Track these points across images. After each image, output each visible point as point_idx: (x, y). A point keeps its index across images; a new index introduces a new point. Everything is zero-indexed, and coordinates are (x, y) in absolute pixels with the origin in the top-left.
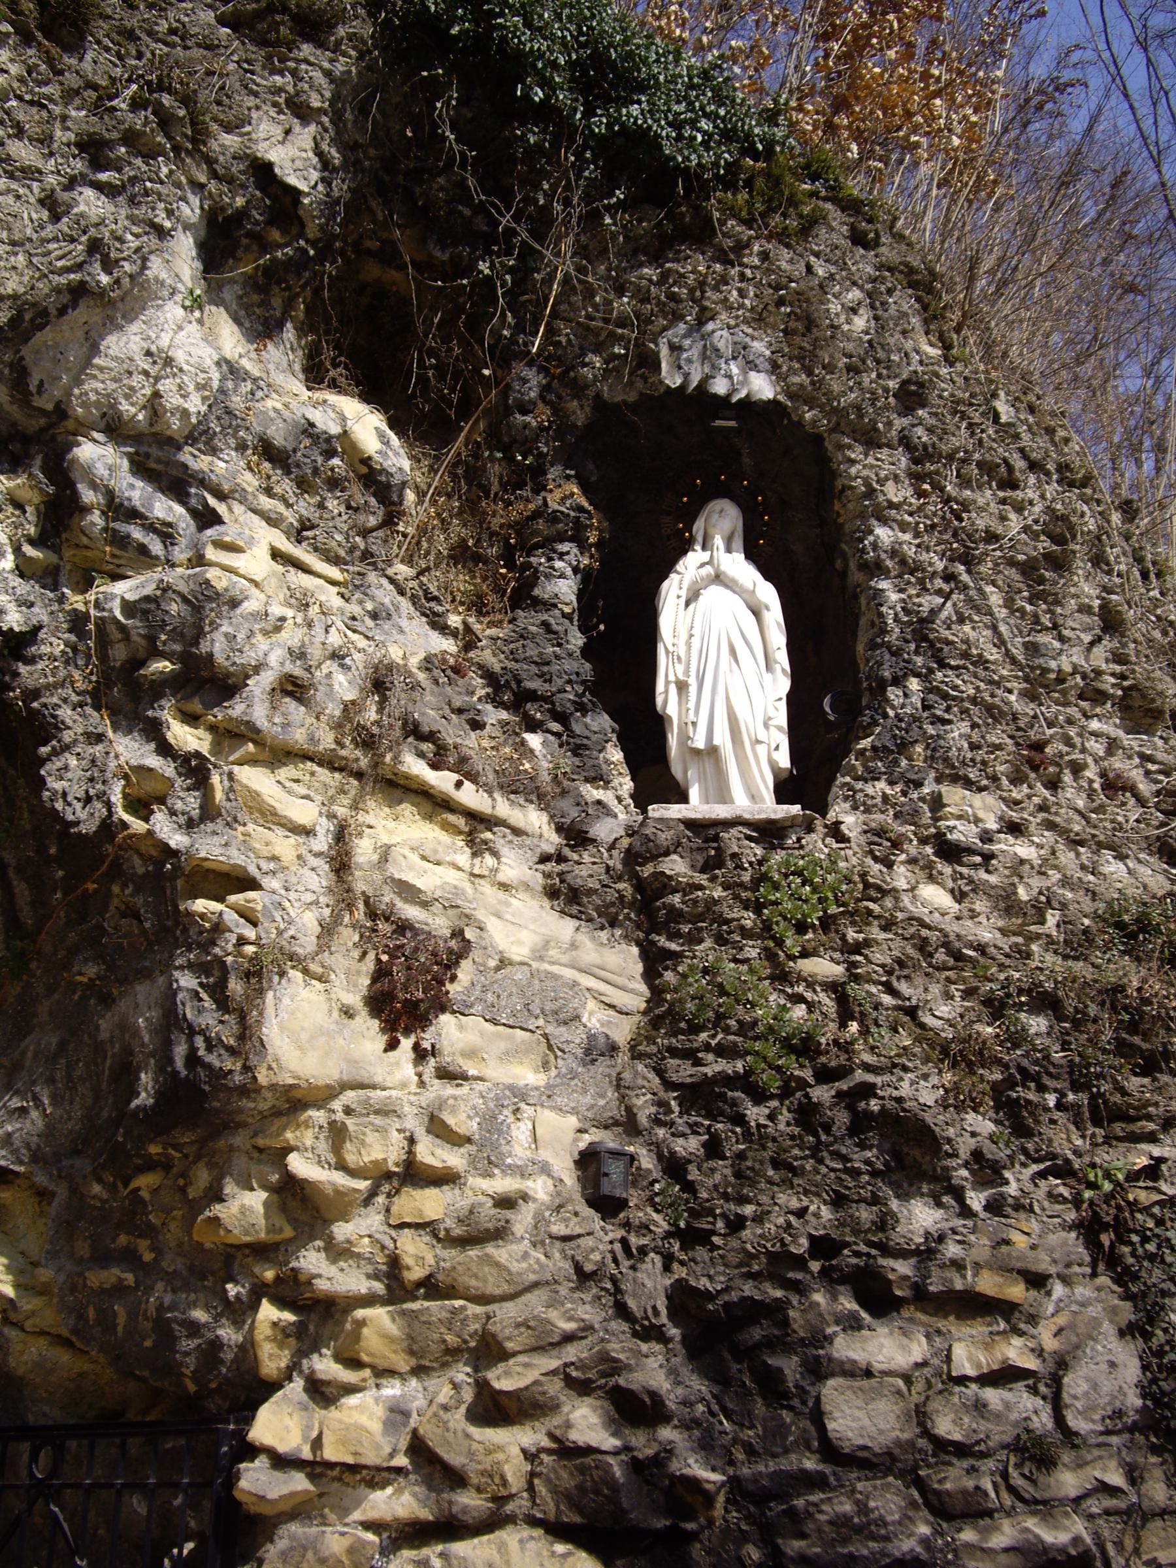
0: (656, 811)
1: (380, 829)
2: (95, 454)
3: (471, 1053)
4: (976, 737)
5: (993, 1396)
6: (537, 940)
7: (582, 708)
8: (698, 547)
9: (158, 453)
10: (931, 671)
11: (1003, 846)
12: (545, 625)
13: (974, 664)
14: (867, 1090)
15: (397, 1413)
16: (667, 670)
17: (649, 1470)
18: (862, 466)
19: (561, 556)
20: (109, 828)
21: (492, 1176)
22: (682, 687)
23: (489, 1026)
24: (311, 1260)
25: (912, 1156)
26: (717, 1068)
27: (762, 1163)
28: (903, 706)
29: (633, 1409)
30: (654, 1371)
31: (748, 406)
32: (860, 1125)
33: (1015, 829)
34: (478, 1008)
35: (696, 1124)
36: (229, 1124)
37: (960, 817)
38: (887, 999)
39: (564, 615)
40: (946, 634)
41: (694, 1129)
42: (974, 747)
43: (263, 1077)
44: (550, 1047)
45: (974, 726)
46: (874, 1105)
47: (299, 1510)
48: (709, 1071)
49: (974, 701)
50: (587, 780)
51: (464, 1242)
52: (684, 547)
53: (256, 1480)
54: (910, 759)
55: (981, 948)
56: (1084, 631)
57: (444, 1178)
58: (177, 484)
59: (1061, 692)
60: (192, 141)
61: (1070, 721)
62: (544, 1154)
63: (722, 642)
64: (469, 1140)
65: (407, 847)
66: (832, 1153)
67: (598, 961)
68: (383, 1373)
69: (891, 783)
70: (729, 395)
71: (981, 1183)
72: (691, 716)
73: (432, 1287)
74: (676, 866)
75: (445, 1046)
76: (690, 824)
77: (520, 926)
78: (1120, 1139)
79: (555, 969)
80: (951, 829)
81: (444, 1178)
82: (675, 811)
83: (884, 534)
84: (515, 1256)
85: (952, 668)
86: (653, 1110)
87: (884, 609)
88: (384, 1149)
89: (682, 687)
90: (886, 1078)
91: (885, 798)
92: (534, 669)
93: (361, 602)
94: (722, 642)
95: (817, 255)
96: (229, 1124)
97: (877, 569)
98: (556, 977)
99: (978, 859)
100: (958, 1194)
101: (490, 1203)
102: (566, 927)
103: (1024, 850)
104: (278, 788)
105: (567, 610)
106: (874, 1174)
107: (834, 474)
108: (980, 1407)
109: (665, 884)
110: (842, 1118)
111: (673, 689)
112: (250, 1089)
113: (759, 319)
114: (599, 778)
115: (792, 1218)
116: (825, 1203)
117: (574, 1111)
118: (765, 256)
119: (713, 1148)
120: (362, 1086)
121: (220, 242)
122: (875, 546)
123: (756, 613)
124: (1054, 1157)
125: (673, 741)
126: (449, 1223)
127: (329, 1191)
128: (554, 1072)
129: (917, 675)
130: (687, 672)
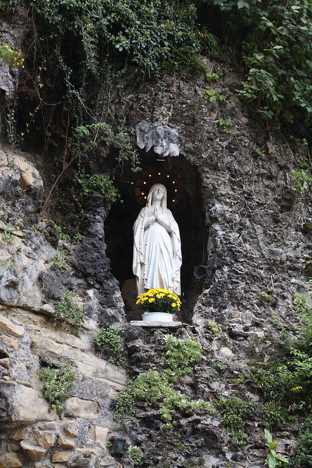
0: (134, 323)
1: (42, 332)
3: (76, 410)
4: (247, 289)
6: (94, 369)
7: (107, 278)
8: (149, 204)
10: (232, 264)
11: (252, 332)
12: (93, 244)
13: (248, 259)
14: (198, 421)
16: (137, 258)
18: (210, 179)
19: (98, 213)
21: (83, 448)
22: (142, 264)
23: (81, 400)
26: (151, 413)
27: (165, 443)
28: (221, 278)
31: (171, 158)
32: (195, 432)
33: (257, 325)
34: (77, 394)
35: (145, 430)
37: (237, 322)
38: (207, 389)
39: (100, 239)
40: (239, 249)
41: (144, 432)
42: (246, 292)
43: (13, 419)
44: (99, 405)
45: (247, 284)
46: (199, 426)
48: (149, 413)
49: (247, 274)
50: (109, 307)
52: (144, 204)
54: (223, 297)
55: (240, 370)
56: (294, 241)
57: (69, 448)
59: (281, 268)
61: (284, 279)
62: (98, 441)
63: (157, 247)
64: (76, 437)
65: (51, 340)
66: (186, 441)
67: (114, 376)
69: (215, 308)
70: (162, 155)
71: (230, 450)
72: (146, 277)
74: (139, 343)
75: (68, 407)
76: (144, 327)
77: (89, 365)
78: (277, 437)
79: (100, 379)
80: (234, 327)
82: (139, 323)
83: (218, 206)
85: (240, 262)
86: (131, 425)
87: (216, 238)
89: (142, 264)
90: (204, 417)
91: (213, 313)
92: (90, 264)
93: (31, 245)
94: (157, 247)
95: (199, 86)
97: (215, 220)
98: (100, 382)
99: (242, 338)
100: (224, 454)
101: (82, 456)
102: (102, 364)
103: (261, 334)
104: (11, 322)
105: (101, 237)
106: (198, 447)
107: (201, 181)
109: (135, 349)
110: (189, 429)
111: (139, 265)
112: (9, 421)
113: (173, 121)
114: (113, 306)
115: (173, 461)
116: (183, 456)
117: (107, 427)
118: (179, 88)
119: (150, 437)
120: (43, 420)
122: (215, 210)
123: (170, 233)
124: (256, 442)
125: (139, 284)
126: (70, 462)
127: (35, 454)
128: (100, 413)
129: (227, 265)
130: (144, 258)
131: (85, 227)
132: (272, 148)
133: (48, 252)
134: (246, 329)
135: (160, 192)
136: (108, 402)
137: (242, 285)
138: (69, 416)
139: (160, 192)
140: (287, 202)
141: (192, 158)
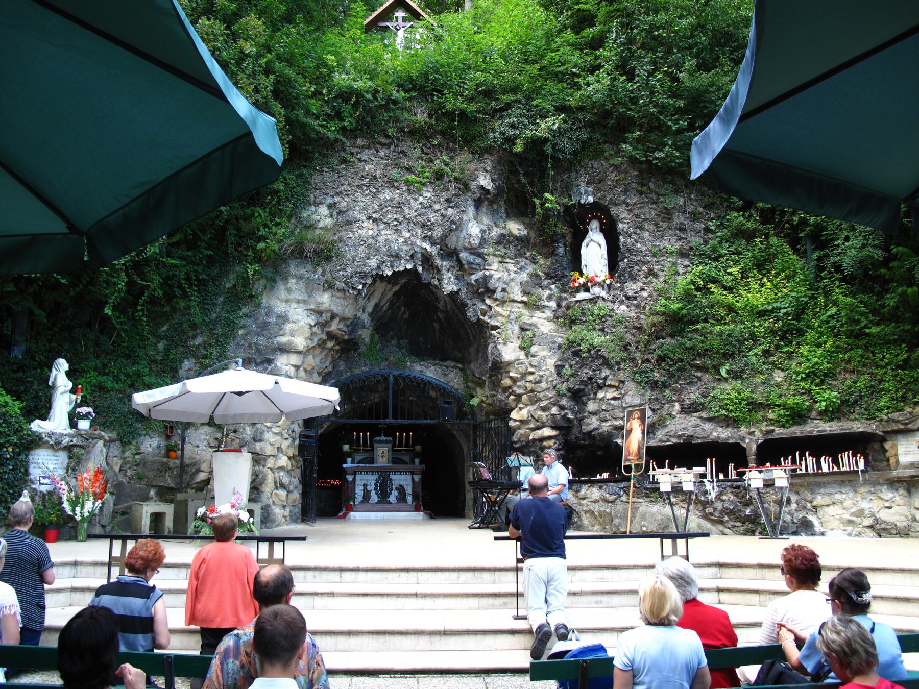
2: (464, 255)
5: (612, 402)
9: (473, 251)
15: (529, 411)
17: (564, 417)
18: (614, 211)
20: (479, 319)
24: (515, 389)
25: (606, 363)
29: (562, 408)
30: (564, 402)
36: (500, 368)
47: (519, 428)
51: (535, 383)
53: (512, 424)
57: (532, 373)
58: (480, 255)
60: (466, 188)
63: (594, 253)
65: (527, 317)
68: (527, 405)
73: (532, 391)
81: (532, 373)
84: (543, 385)
88: (522, 369)
94: (594, 253)
96: (500, 368)
97: (620, 234)
108: (610, 404)
113: (588, 183)
121: (478, 204)
131: (553, 253)
132: (652, 185)
133: (530, 269)
134: (636, 293)
135: (595, 224)
136: (556, 345)
137: (637, 267)
138: (533, 356)
139: (595, 224)
140: (667, 215)
141: (602, 202)
